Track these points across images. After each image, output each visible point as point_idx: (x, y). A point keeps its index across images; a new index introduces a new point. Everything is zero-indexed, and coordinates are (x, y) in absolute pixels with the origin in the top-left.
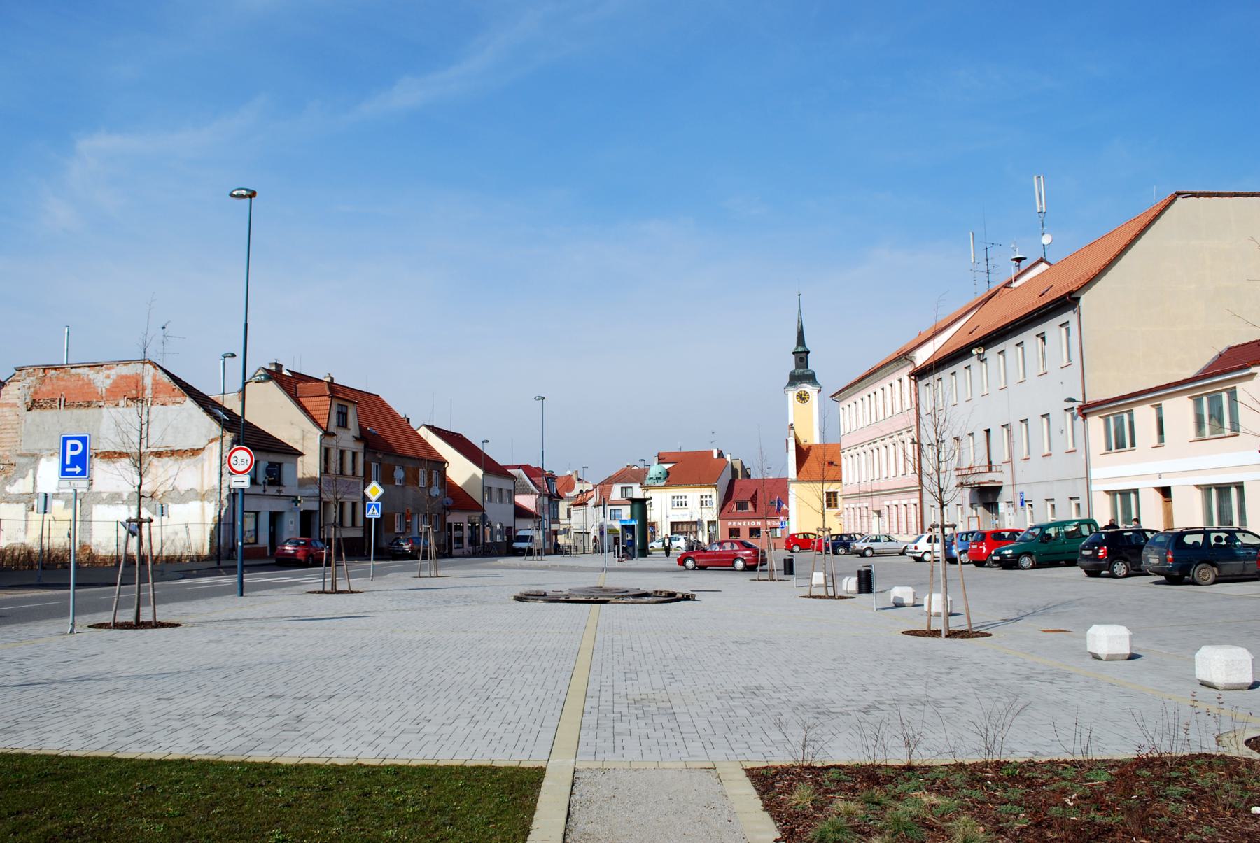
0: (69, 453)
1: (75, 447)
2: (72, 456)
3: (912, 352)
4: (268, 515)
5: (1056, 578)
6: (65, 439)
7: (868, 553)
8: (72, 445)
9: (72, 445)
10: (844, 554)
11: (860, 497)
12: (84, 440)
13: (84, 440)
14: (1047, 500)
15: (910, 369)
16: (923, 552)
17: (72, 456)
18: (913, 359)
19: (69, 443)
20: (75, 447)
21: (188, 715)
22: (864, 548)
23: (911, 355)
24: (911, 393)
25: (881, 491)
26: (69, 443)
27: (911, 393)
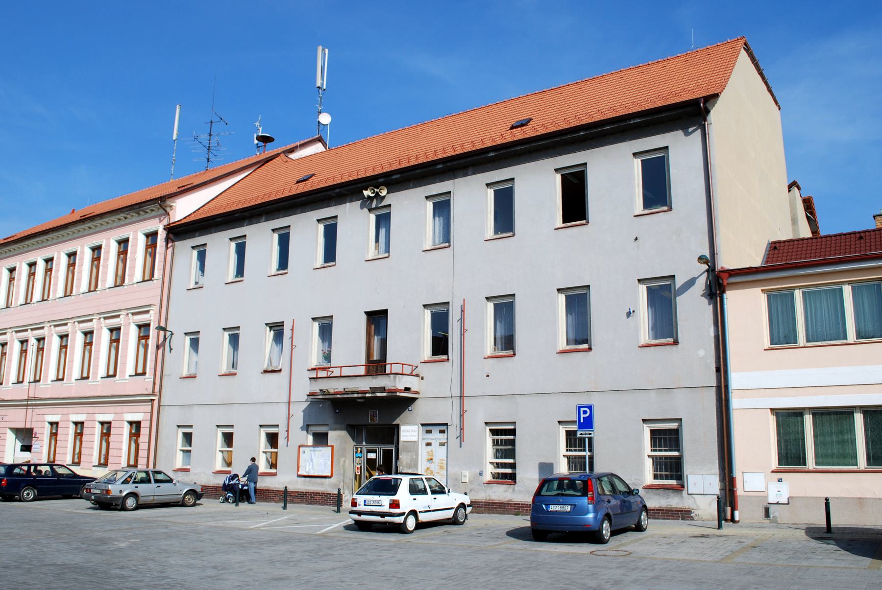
0: (582, 416)
1: (585, 412)
2: (584, 417)
3: (170, 199)
4: (277, 432)
5: (420, 567)
6: (579, 408)
7: (131, 502)
8: (583, 411)
9: (583, 411)
10: (34, 500)
11: (27, 405)
12: (590, 408)
13: (590, 408)
14: (218, 426)
15: (165, 222)
16: (456, 506)
17: (584, 417)
18: (168, 209)
19: (582, 410)
20: (585, 412)
21: (171, 578)
22: (124, 494)
23: (168, 202)
24: (8, 238)
25: (41, 399)
26: (582, 410)
27: (8, 238)
